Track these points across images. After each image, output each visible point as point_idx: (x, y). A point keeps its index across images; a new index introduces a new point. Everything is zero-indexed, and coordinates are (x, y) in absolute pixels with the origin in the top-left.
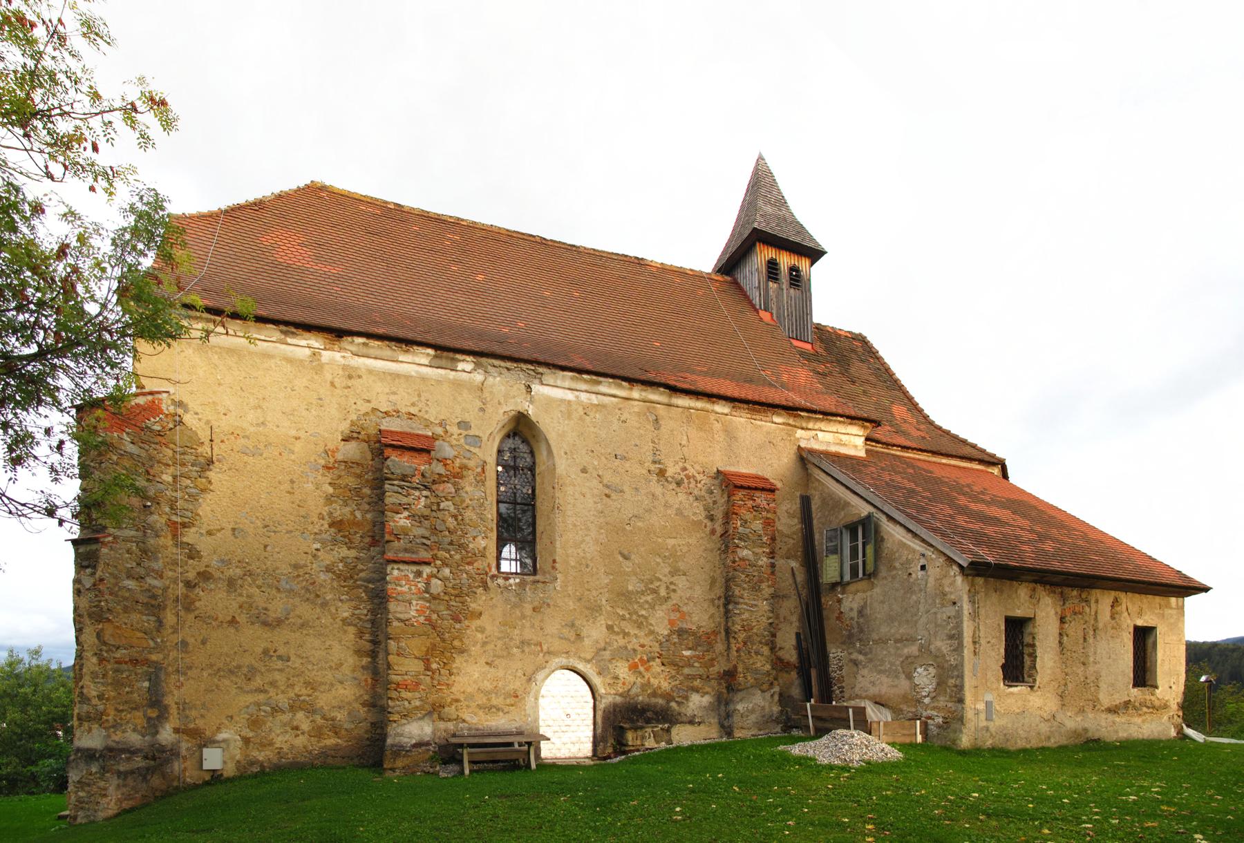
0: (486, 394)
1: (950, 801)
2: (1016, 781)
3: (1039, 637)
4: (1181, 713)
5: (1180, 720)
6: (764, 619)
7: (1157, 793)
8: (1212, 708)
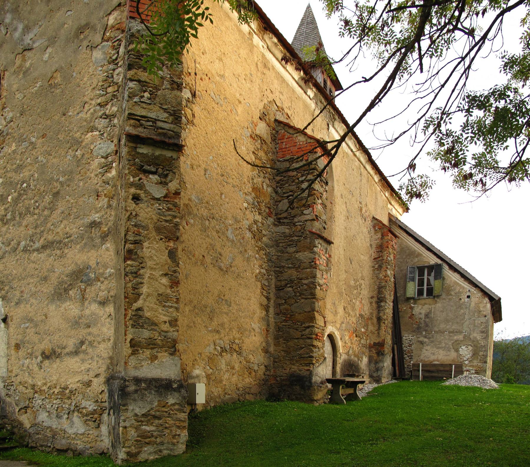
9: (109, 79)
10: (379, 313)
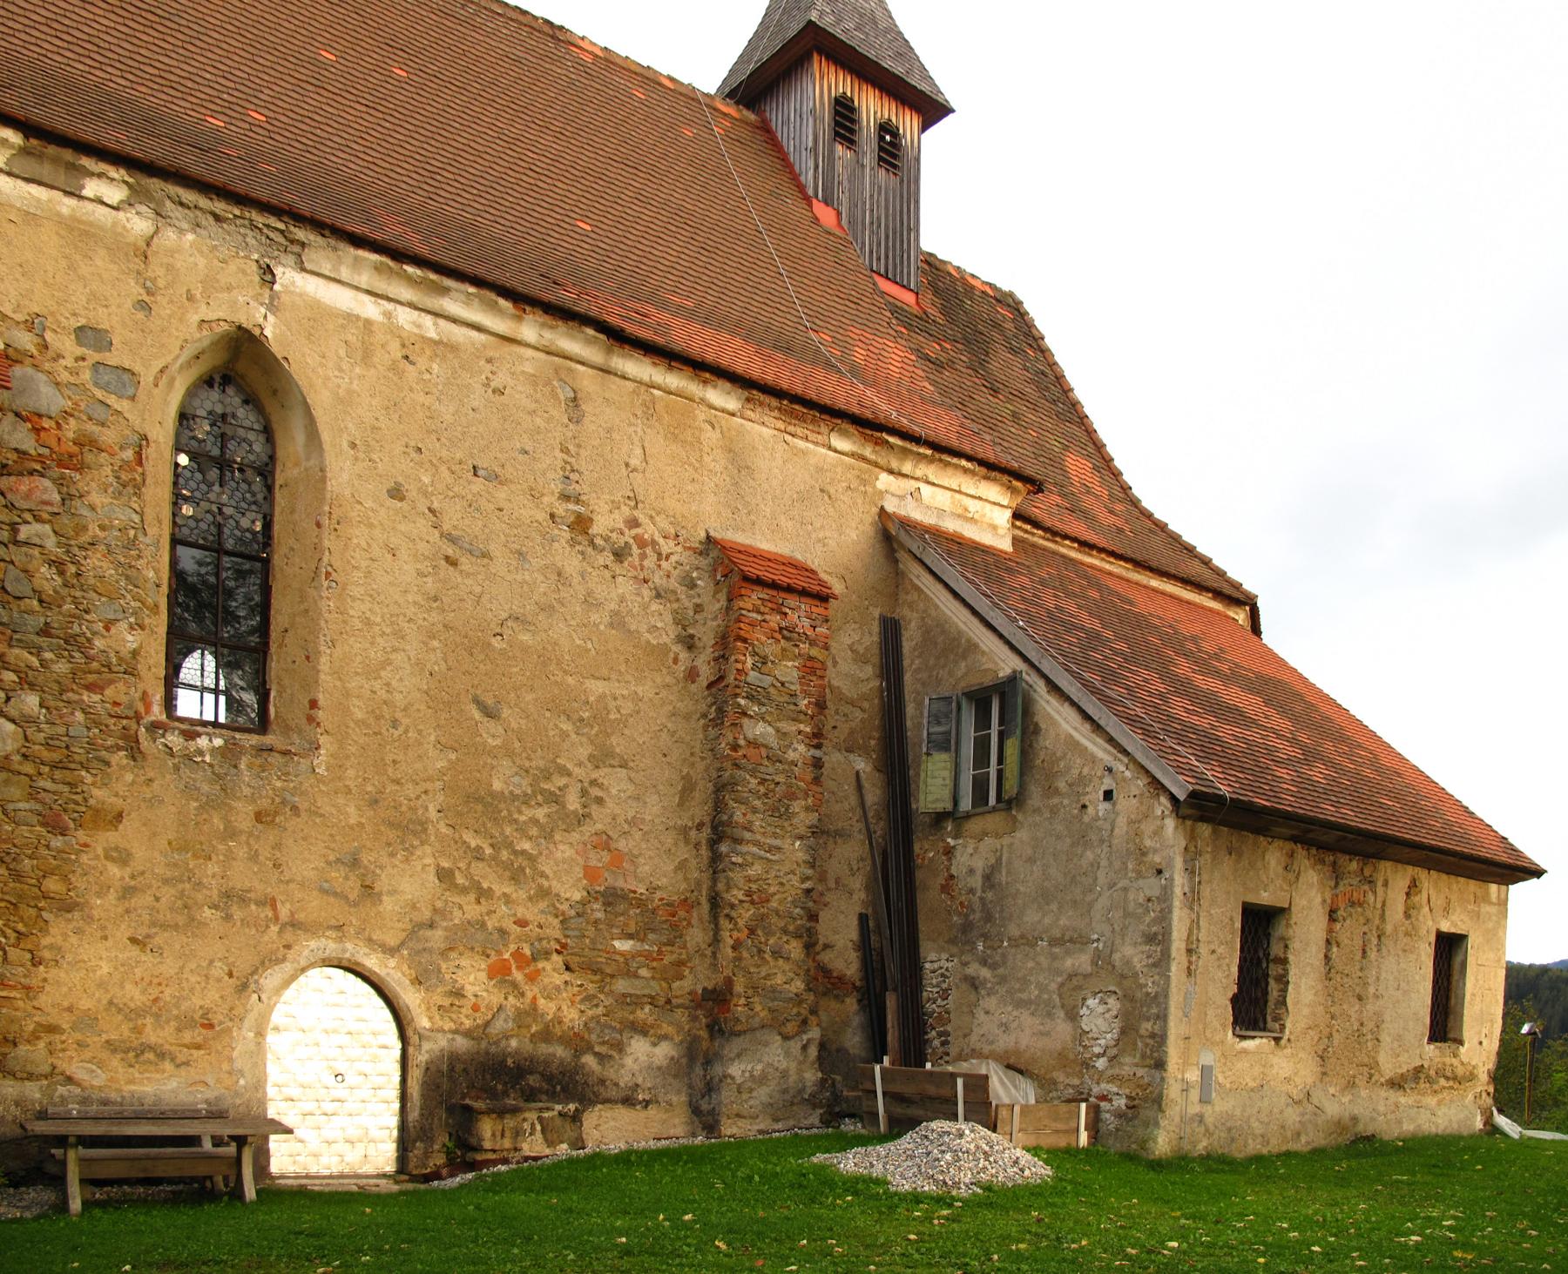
0: (156, 270)
1: (1129, 1257)
2: (1241, 1216)
3: (1295, 945)
4: (1491, 1090)
5: (1490, 1101)
6: (795, 881)
7: (1450, 1229)
8: (1534, 1081)
10: (714, 881)
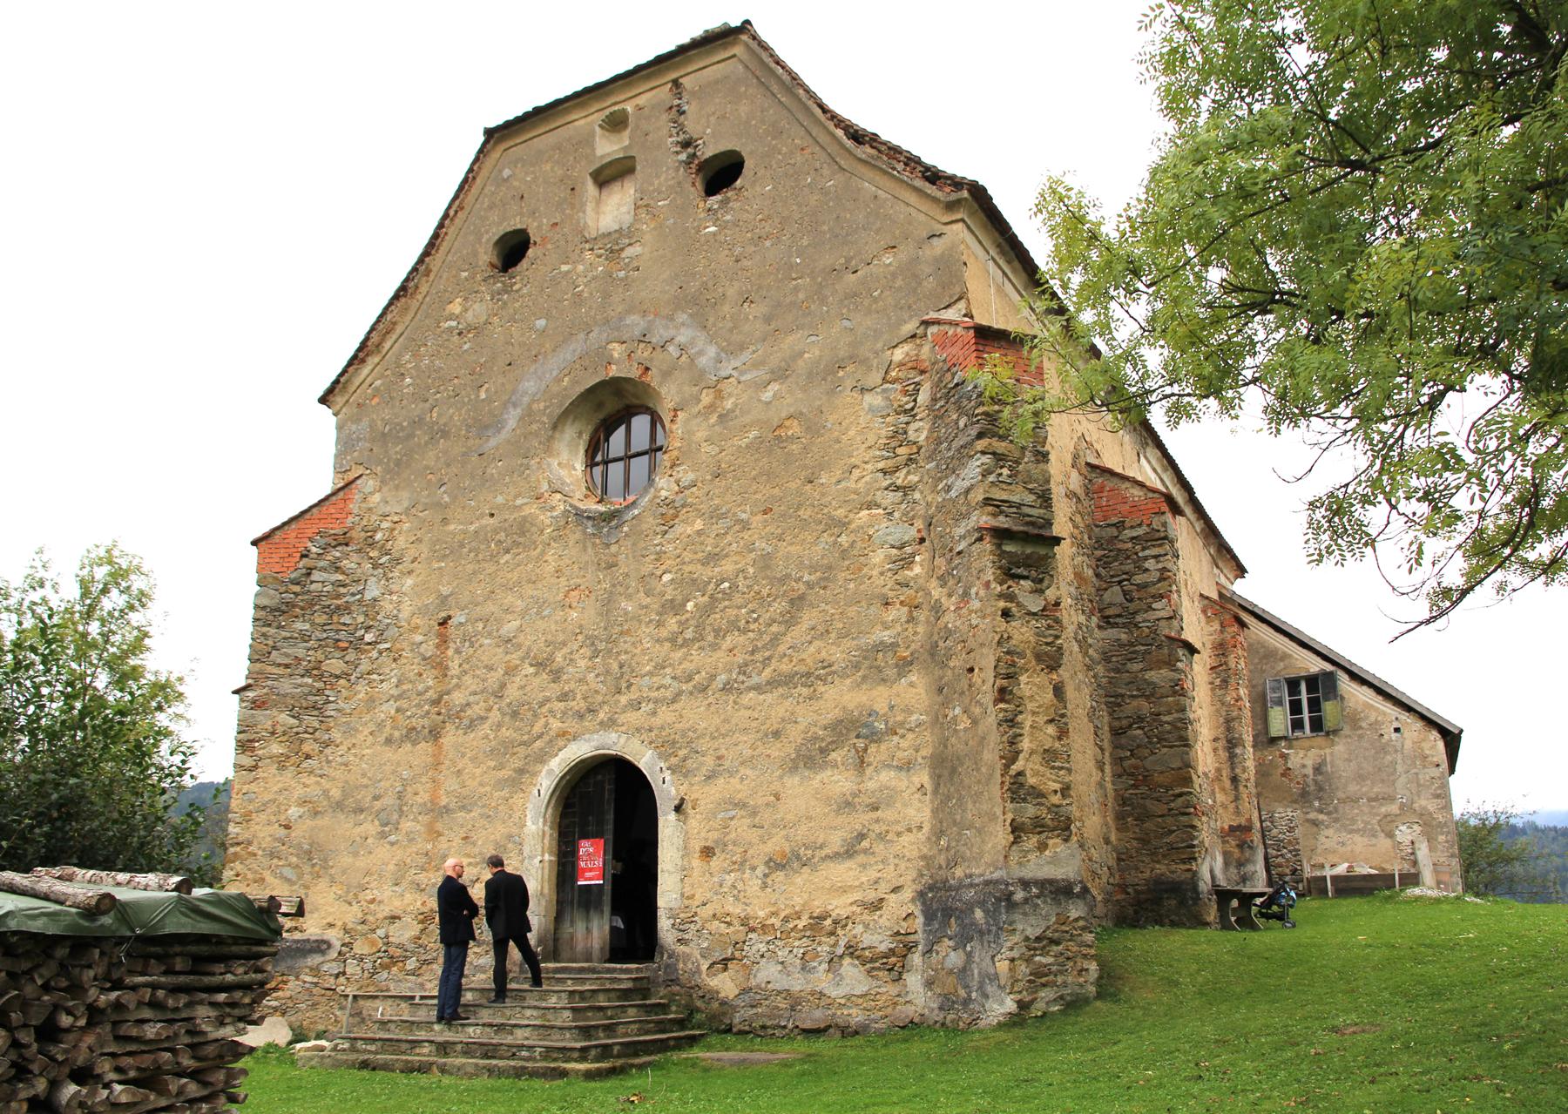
9: (899, 435)
10: (1233, 769)
